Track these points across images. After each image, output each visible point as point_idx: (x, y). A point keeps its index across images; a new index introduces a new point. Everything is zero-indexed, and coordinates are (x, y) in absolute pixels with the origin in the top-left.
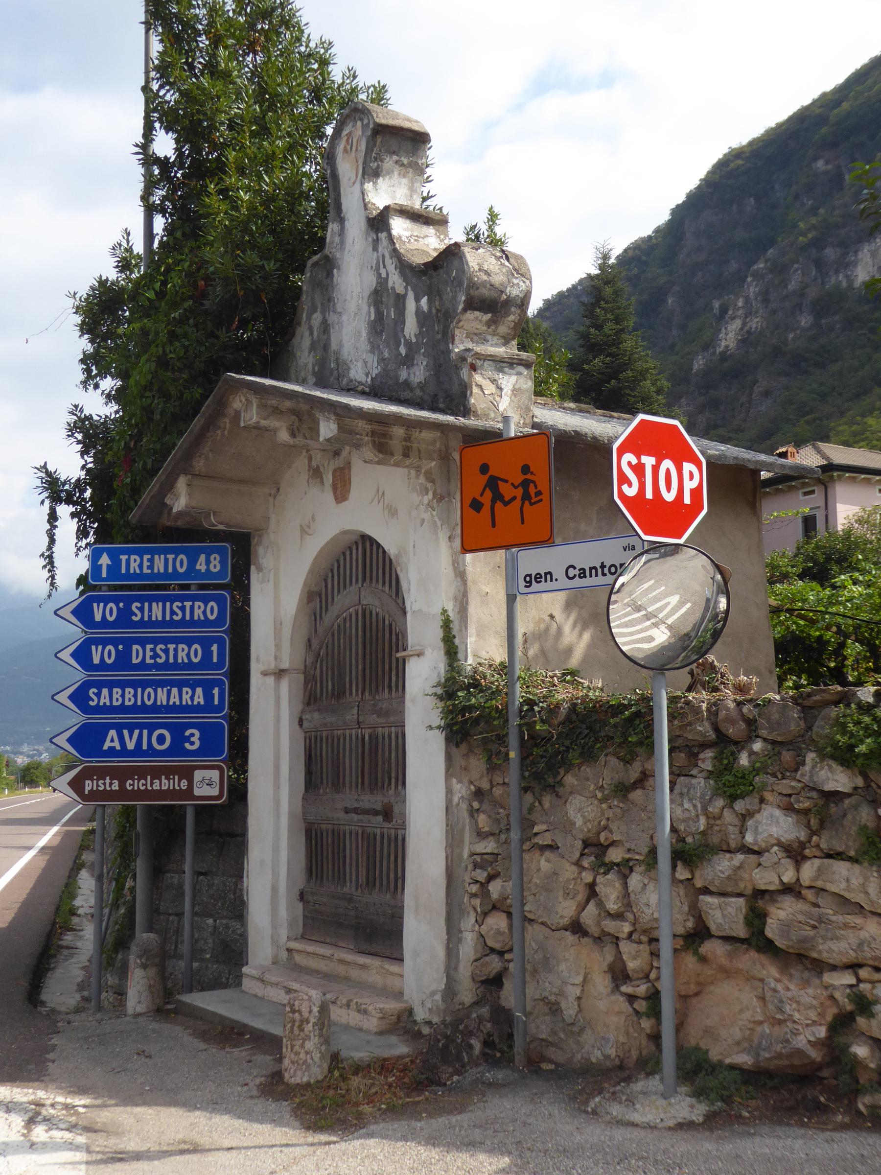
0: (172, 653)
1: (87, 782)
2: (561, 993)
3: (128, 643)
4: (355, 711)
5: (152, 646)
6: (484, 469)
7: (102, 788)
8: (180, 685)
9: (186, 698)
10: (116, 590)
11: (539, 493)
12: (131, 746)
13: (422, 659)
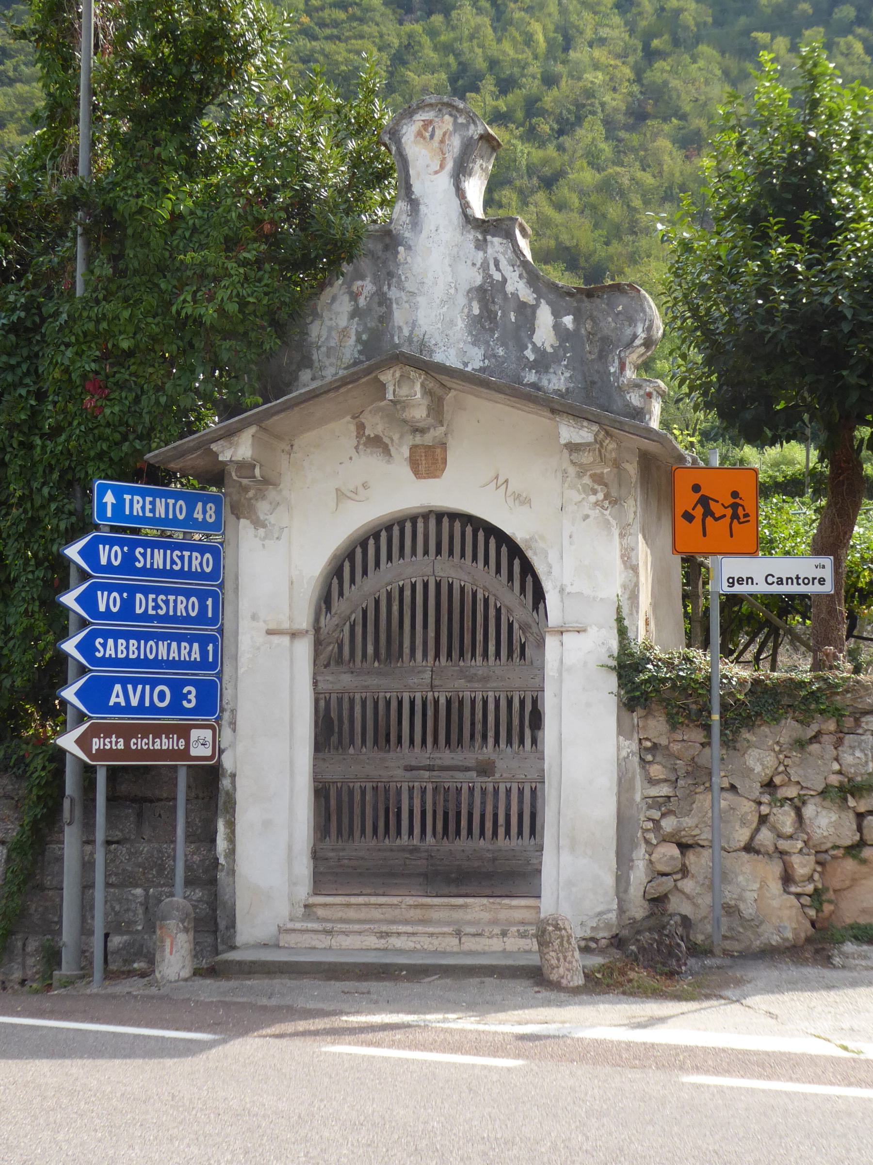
0: (171, 604)
1: (95, 740)
2: (741, 898)
3: (133, 590)
4: (428, 675)
5: (154, 596)
6: (696, 488)
7: (108, 747)
8: (179, 638)
9: (184, 652)
10: (117, 532)
11: (746, 515)
12: (134, 702)
13: (582, 635)
